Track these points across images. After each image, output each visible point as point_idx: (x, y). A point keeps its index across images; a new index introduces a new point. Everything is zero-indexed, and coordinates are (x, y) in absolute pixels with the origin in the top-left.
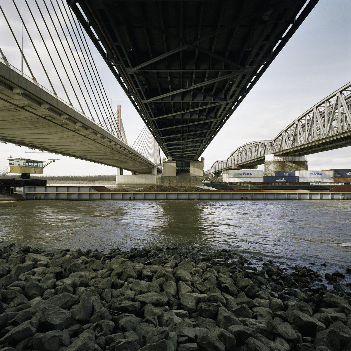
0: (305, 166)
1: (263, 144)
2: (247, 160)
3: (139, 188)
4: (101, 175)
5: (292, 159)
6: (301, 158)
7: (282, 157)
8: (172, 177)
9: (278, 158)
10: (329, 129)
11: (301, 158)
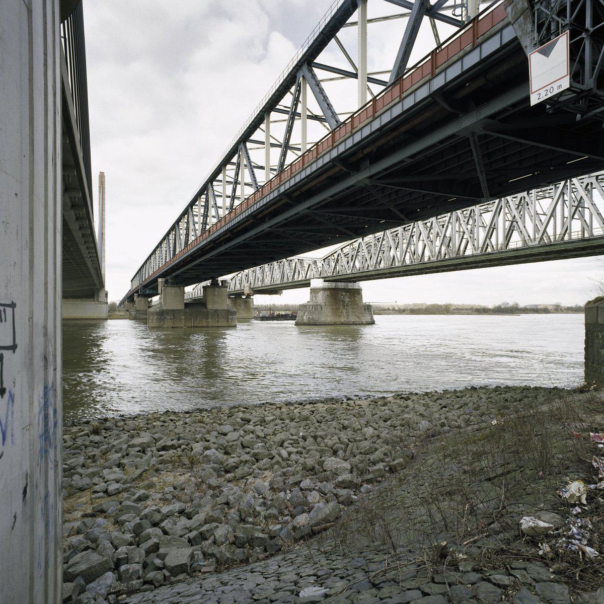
2: (236, 289)
3: (184, 273)
8: (178, 310)
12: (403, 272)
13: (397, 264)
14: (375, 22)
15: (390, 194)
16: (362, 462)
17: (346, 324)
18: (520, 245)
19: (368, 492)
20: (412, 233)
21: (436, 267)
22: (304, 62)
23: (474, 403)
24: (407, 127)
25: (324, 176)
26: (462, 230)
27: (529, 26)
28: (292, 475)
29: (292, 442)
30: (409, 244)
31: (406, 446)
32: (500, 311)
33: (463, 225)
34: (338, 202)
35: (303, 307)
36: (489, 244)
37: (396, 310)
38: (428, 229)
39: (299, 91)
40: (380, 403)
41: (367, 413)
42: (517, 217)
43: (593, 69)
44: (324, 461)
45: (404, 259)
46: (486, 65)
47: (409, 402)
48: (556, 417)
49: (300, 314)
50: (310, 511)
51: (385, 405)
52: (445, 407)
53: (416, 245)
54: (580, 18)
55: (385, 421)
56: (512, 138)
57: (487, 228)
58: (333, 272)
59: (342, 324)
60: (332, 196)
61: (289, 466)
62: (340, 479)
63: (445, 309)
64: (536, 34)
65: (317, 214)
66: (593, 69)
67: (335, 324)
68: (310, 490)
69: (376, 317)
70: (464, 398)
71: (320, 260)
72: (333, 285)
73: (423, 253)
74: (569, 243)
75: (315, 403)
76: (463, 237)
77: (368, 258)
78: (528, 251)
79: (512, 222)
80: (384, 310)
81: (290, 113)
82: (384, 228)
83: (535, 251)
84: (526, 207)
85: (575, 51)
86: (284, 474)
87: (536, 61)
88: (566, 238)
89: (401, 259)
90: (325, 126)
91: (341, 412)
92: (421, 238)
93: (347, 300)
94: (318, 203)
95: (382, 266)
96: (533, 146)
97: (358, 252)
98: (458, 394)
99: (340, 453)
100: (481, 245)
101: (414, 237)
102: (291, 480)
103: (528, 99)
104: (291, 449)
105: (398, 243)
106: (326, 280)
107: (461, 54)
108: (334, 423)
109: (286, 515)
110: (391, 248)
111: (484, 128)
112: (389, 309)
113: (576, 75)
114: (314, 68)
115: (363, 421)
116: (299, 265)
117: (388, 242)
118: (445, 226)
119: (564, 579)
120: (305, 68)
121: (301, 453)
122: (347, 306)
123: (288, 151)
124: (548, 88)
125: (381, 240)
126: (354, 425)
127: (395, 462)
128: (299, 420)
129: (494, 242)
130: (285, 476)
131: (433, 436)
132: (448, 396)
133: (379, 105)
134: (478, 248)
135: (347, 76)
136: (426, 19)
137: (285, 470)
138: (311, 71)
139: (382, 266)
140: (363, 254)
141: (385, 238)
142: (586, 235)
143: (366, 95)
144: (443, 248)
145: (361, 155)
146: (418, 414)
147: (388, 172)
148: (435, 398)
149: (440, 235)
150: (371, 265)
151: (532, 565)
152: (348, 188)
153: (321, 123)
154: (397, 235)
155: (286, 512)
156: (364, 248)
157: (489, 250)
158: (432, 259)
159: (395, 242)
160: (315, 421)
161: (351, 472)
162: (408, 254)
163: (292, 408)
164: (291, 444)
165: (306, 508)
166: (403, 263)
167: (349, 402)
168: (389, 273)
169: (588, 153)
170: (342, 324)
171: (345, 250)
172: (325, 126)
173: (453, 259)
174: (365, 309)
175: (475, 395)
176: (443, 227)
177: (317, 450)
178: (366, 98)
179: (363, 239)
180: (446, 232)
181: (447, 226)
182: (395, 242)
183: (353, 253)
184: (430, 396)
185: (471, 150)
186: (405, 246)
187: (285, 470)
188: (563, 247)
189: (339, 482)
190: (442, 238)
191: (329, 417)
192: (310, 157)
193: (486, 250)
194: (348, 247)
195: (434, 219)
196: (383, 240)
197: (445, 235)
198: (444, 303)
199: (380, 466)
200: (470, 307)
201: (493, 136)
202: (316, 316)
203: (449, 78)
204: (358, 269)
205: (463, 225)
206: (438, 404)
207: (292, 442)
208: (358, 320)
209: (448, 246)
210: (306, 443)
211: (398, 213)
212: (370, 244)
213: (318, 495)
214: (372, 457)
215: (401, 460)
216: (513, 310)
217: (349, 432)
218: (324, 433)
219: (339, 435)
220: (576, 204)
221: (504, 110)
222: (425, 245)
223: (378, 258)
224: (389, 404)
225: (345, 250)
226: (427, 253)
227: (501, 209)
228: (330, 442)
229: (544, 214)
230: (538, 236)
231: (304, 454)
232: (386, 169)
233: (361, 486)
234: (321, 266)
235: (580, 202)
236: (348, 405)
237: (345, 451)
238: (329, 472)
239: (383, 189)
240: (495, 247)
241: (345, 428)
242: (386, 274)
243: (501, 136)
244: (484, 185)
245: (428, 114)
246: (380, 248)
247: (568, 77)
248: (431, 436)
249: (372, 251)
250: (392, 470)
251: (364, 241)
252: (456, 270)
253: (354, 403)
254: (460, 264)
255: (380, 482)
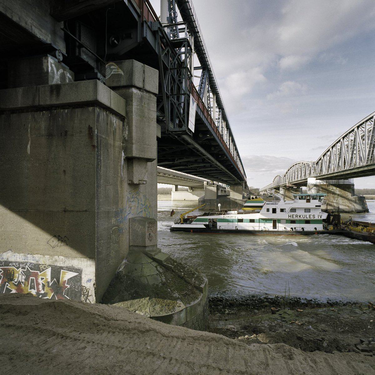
0: (350, 190)
1: (306, 165)
4: (163, 188)
5: (336, 182)
6: (346, 182)
7: (325, 181)
8: (213, 200)
9: (321, 182)
10: (352, 155)
11: (346, 182)
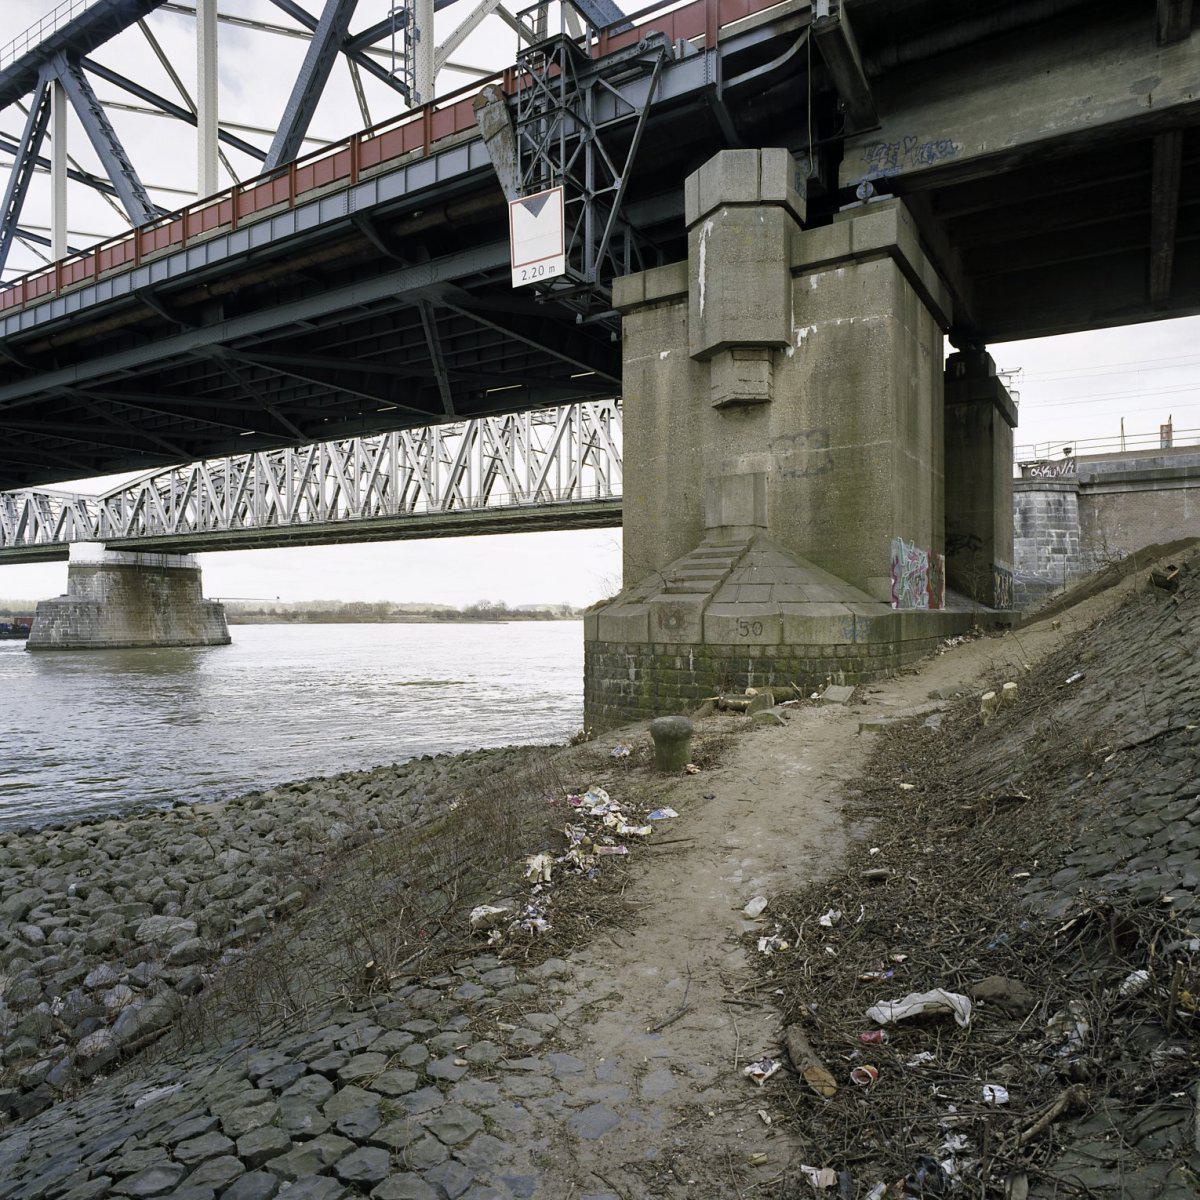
12: (295, 537)
13: (281, 521)
14: (233, 23)
15: (267, 382)
16: (219, 911)
17: (161, 646)
18: (506, 501)
19: (238, 959)
20: (312, 459)
21: (360, 532)
22: (59, 49)
23: (426, 783)
24: (304, 262)
25: (115, 323)
26: (408, 465)
27: (511, 154)
28: (60, 969)
29: (52, 905)
30: (305, 482)
31: (305, 872)
32: (475, 615)
33: (411, 454)
34: (148, 381)
35: (49, 608)
36: (457, 495)
37: (276, 614)
38: (346, 455)
39: (46, 111)
40: (249, 804)
41: (222, 826)
42: (502, 452)
43: (596, 251)
44: (137, 927)
45: (296, 510)
46: (444, 194)
47: (309, 796)
48: (533, 785)
49: (39, 623)
50: (112, 1024)
51: (261, 805)
52: (377, 796)
53: (320, 485)
54: (579, 169)
55: (262, 835)
56: (488, 323)
57: (453, 466)
58: (130, 530)
59: (154, 645)
60: (135, 369)
61: (48, 953)
62: (176, 949)
63: (377, 613)
64: (520, 175)
65: (93, 400)
66: (596, 251)
67: (134, 646)
68: (110, 986)
69: (233, 631)
70: (410, 777)
71: (95, 500)
72: (130, 558)
73: (335, 501)
74: (577, 504)
75: (97, 822)
76: (410, 477)
77: (216, 501)
78: (518, 512)
79: (494, 459)
80: (250, 614)
81: (20, 153)
82: (253, 446)
83: (528, 514)
84: (516, 435)
85: (572, 214)
86: (40, 972)
87: (518, 213)
88: (575, 495)
89: (289, 510)
90: (112, 203)
91: (165, 831)
92: (331, 472)
93: (165, 592)
94: (98, 378)
95: (248, 522)
96: (519, 343)
97: (192, 488)
98: (400, 771)
99: (171, 906)
100: (442, 496)
101: (318, 468)
102: (60, 978)
103: (507, 269)
104: (49, 921)
105: (283, 478)
106: (111, 545)
107: (404, 159)
108: (151, 854)
109: (57, 1044)
110: (267, 486)
111: (445, 298)
112: (261, 613)
113: (574, 254)
114: (85, 71)
115: (216, 841)
116: (35, 509)
117: (262, 473)
118: (378, 453)
119: (511, 962)
120: (61, 64)
121: (78, 924)
122: (166, 605)
123: (15, 241)
124: (536, 265)
125: (246, 467)
126: (197, 852)
127: (287, 900)
128: (61, 861)
129: (465, 495)
130: (43, 974)
131: (355, 846)
132: (383, 776)
133: (247, 203)
134: (438, 500)
135: (169, 112)
136: (341, 59)
137: (38, 964)
138: (80, 77)
139: (248, 522)
140: (204, 494)
141: (254, 464)
142: (603, 494)
143: (215, 171)
144: (374, 497)
145: (205, 296)
146: (327, 813)
147: (264, 340)
148: (359, 782)
149: (368, 467)
150: (223, 518)
151: (480, 960)
152: (173, 358)
153: (103, 194)
154: (280, 461)
155: (56, 1038)
156: (207, 480)
157: (456, 506)
158: (352, 515)
159: (277, 475)
160: (103, 856)
161: (199, 933)
162: (303, 501)
163: (38, 839)
164: (50, 911)
165: (102, 1019)
166: (293, 520)
167: (179, 810)
168: (263, 539)
169: (594, 367)
170: (154, 645)
171: (161, 483)
172: (112, 203)
173: (393, 518)
174: (208, 613)
175: (429, 769)
176: (374, 454)
177: (116, 911)
178: (215, 183)
179: (204, 464)
180: (379, 464)
181: (382, 454)
182: (277, 475)
183: (179, 490)
184: (349, 780)
185: (421, 328)
186: (297, 485)
187: (38, 964)
188: (569, 511)
189: (174, 957)
190: (371, 475)
191: (136, 845)
192: (78, 270)
193: (451, 506)
194: (169, 476)
195: (357, 440)
196: (251, 467)
197: (377, 470)
198: (376, 601)
199: (259, 910)
200: (421, 610)
201: (456, 313)
202: (84, 630)
203: (385, 197)
204: (192, 525)
205: (411, 454)
206: (363, 792)
207: (52, 905)
208: (192, 637)
209: (384, 492)
210: (87, 902)
211: (283, 420)
212: (221, 474)
213: (129, 991)
214: (240, 901)
215: (298, 894)
216: (498, 615)
217: (189, 868)
218: (131, 876)
219: (164, 874)
220: (588, 441)
221: (474, 277)
222: (339, 488)
223: (238, 505)
224: (268, 804)
225: (161, 483)
226: (343, 504)
227: (476, 433)
228: (146, 891)
229: (543, 452)
230: (534, 488)
231: (84, 926)
232: (261, 334)
233: (221, 953)
234: (98, 513)
235: (593, 438)
236: (179, 815)
237: (181, 902)
238: (150, 945)
239: (253, 369)
240: (465, 500)
241: (174, 860)
242: (256, 539)
243: (472, 316)
244: (445, 393)
245: (343, 249)
246: (244, 485)
247: (563, 257)
248: (350, 846)
249: (225, 489)
250: (281, 914)
251: (208, 467)
252: (397, 538)
253: (193, 811)
254: (406, 528)
255: (256, 939)
